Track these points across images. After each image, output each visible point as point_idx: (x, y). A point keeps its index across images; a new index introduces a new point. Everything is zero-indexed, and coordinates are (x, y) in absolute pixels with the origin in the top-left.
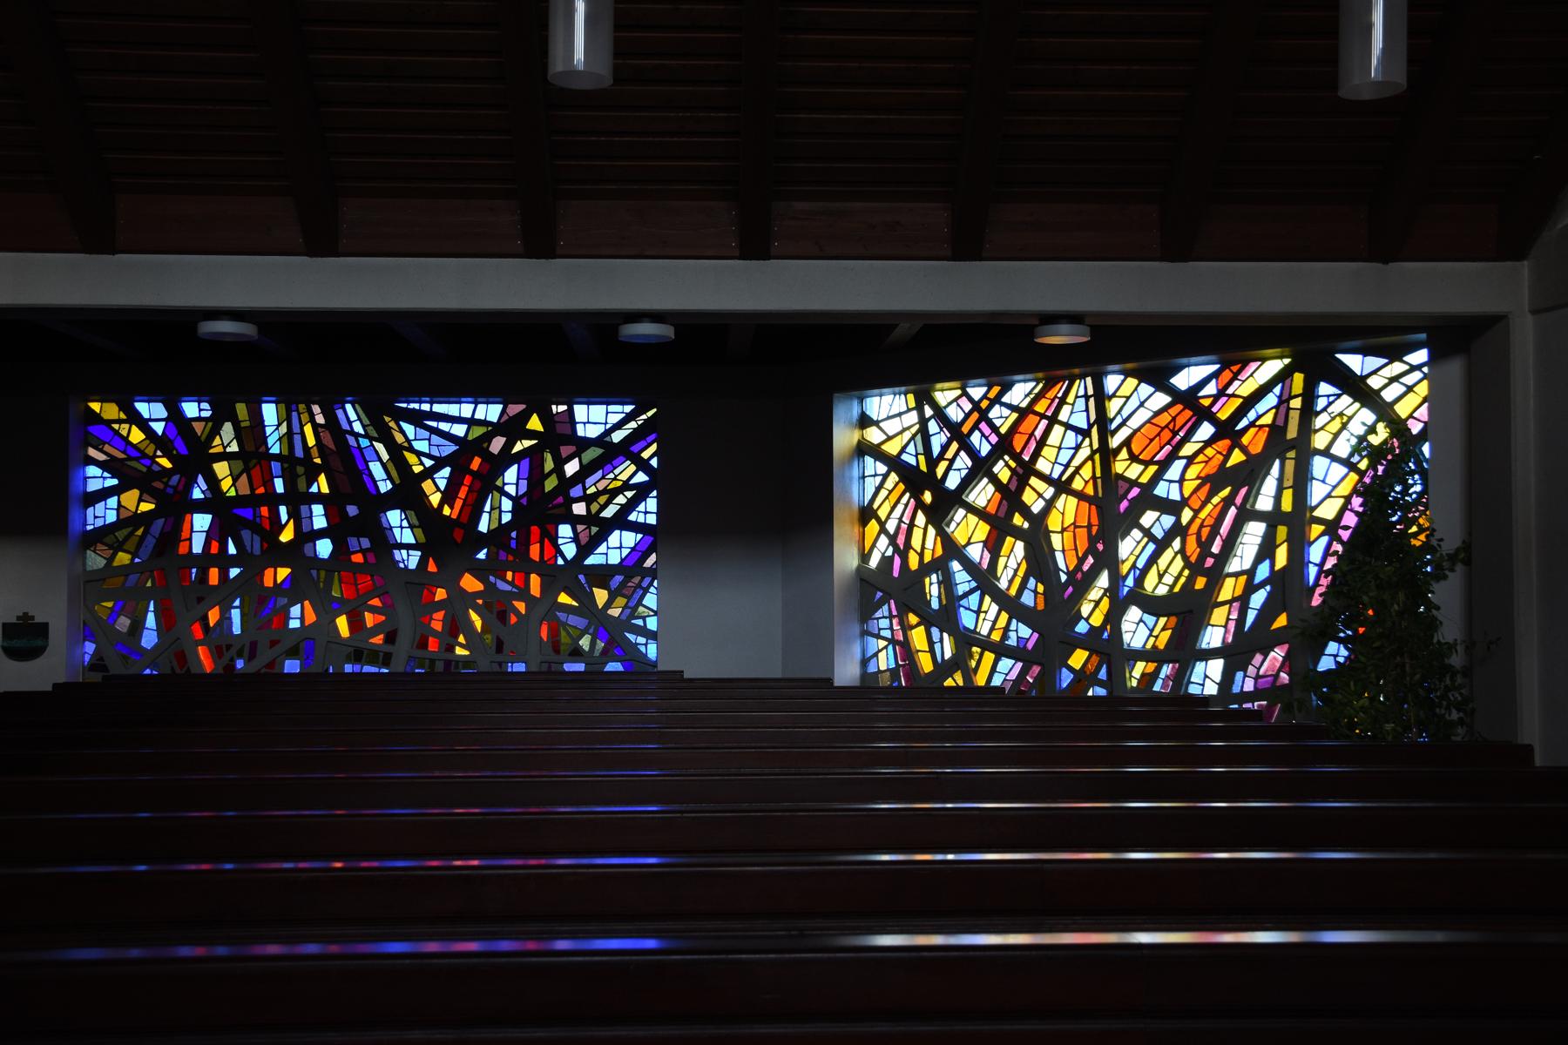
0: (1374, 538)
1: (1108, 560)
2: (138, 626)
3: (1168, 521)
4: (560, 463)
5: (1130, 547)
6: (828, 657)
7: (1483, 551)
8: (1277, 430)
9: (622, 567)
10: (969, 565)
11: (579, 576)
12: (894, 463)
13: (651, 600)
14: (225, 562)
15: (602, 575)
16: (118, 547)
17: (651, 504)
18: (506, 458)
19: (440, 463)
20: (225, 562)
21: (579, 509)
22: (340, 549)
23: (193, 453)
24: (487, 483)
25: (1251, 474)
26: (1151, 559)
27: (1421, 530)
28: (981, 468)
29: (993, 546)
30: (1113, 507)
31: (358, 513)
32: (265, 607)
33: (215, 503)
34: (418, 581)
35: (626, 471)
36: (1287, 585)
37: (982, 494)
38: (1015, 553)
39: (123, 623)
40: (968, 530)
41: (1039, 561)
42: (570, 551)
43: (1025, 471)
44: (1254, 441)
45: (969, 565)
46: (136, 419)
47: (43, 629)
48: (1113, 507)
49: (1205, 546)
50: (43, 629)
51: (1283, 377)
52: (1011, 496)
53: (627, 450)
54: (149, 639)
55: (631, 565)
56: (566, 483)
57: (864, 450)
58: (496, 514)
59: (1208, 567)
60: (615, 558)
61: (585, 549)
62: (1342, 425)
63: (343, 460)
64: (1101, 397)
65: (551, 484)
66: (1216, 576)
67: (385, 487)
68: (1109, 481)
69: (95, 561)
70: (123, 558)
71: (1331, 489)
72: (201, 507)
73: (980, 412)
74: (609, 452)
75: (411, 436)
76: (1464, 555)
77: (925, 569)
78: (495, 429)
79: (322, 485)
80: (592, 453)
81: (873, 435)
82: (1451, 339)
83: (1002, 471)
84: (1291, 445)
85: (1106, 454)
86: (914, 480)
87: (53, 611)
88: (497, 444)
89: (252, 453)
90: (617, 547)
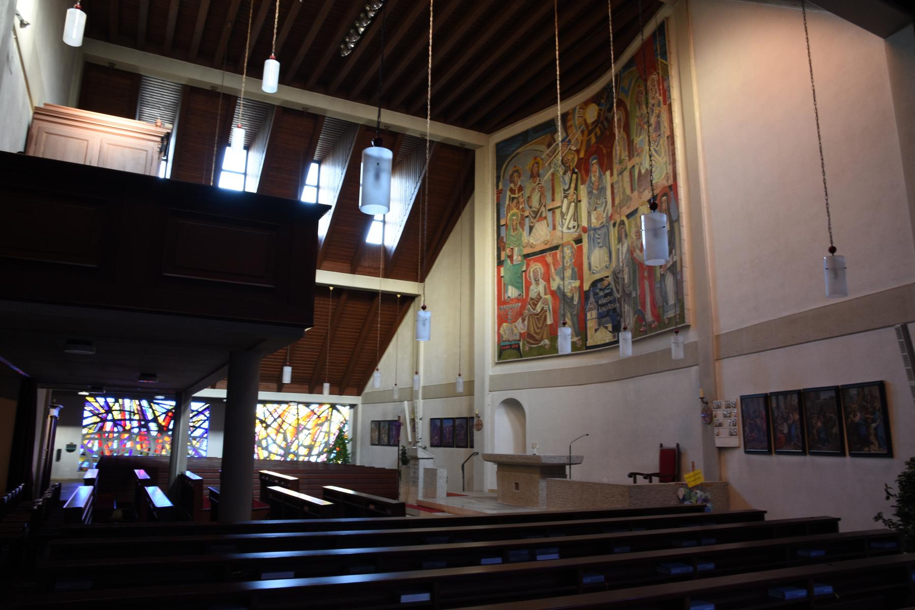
0: (340, 437)
1: (297, 438)
5: (301, 436)
7: (354, 440)
14: (113, 432)
15: (195, 438)
17: (207, 422)
20: (113, 432)
25: (321, 425)
26: (305, 439)
30: (298, 429)
31: (144, 423)
32: (122, 442)
33: (113, 420)
34: (156, 439)
35: (202, 417)
36: (327, 443)
37: (275, 425)
38: (281, 436)
41: (285, 439)
44: (323, 419)
46: (97, 401)
47: (75, 446)
48: (298, 429)
50: (75, 446)
52: (280, 426)
53: (202, 413)
55: (201, 437)
63: (142, 412)
68: (299, 424)
71: (335, 430)
72: (110, 421)
74: (199, 413)
76: (351, 440)
79: (137, 417)
80: (195, 413)
82: (352, 406)
87: (77, 442)
89: (122, 411)
90: (198, 432)
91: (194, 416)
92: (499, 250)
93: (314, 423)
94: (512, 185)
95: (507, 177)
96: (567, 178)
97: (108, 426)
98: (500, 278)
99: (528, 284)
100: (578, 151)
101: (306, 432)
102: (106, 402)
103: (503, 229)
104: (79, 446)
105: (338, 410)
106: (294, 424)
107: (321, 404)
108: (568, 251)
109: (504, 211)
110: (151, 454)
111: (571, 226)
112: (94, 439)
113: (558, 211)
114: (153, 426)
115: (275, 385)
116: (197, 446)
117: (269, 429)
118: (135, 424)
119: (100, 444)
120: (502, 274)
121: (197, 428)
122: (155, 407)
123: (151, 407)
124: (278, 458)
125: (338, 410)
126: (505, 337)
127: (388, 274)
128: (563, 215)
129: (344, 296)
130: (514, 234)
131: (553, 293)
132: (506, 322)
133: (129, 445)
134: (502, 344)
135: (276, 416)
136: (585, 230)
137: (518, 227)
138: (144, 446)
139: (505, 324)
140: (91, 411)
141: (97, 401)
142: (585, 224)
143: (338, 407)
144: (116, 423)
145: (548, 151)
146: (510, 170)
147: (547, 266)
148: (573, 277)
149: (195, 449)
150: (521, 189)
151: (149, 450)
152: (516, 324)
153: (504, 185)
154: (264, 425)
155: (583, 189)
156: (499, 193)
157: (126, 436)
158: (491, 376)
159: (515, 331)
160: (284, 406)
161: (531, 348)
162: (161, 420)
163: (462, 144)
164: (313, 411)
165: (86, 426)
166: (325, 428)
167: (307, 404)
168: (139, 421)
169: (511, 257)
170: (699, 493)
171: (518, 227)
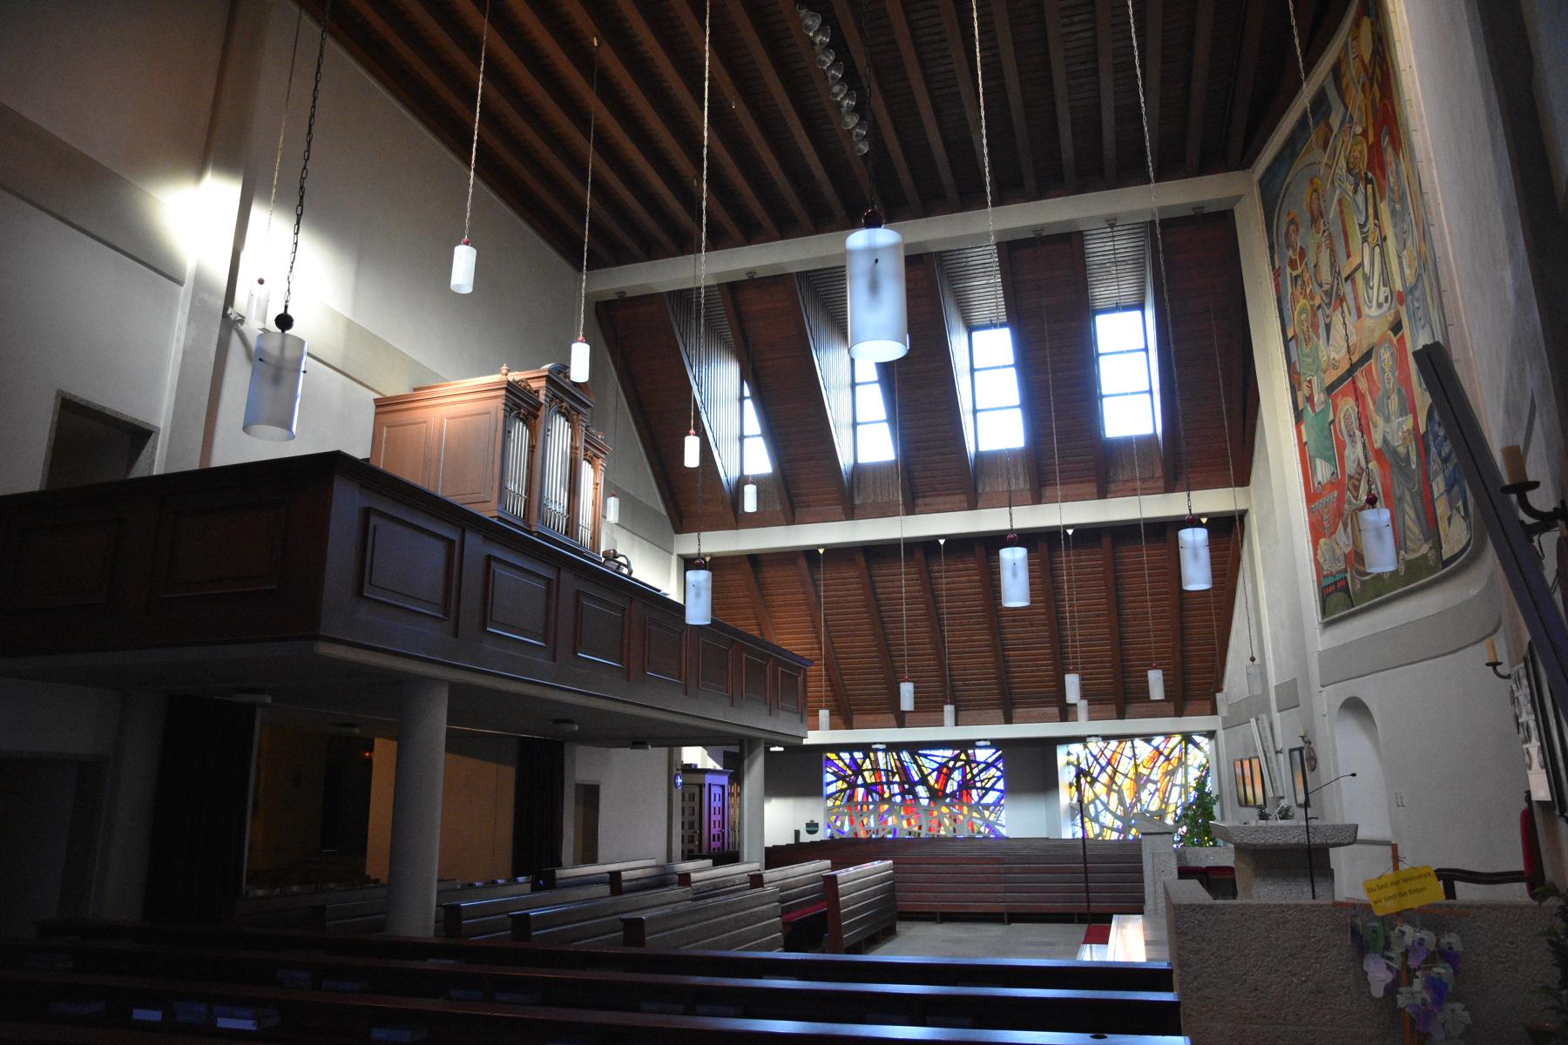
1: (1139, 800)
6: (1060, 832)
15: (987, 807)
18: (954, 768)
22: (903, 798)
23: (858, 770)
24: (948, 777)
25: (1172, 773)
28: (1103, 769)
29: (1108, 794)
30: (1140, 781)
32: (881, 818)
33: (865, 785)
34: (928, 811)
35: (993, 771)
37: (1104, 778)
38: (1114, 796)
40: (1100, 789)
41: (1121, 801)
43: (1115, 771)
44: (1174, 762)
52: (1112, 779)
55: (997, 803)
58: (952, 786)
61: (981, 798)
62: (1196, 758)
63: (903, 771)
66: (1167, 804)
67: (916, 779)
68: (1138, 774)
69: (830, 803)
74: (988, 766)
79: (897, 778)
82: (1211, 735)
83: (1109, 770)
84: (1182, 762)
85: (1136, 766)
87: (820, 819)
89: (875, 770)
90: (992, 797)
92: (1294, 389)
93: (1161, 771)
94: (1290, 253)
95: (1282, 240)
96: (1360, 198)
97: (860, 791)
98: (1302, 446)
99: (1341, 446)
100: (1364, 133)
101: (1151, 787)
102: (852, 758)
103: (1292, 345)
104: (821, 827)
105: (1196, 745)
106: (1131, 775)
107: (1168, 736)
108: (1385, 355)
109: (1287, 306)
111: (1382, 299)
112: (843, 814)
113: (1359, 276)
115: (1055, 710)
118: (896, 789)
119: (852, 822)
121: (987, 790)
122: (922, 761)
123: (916, 762)
124: (1115, 836)
125: (1196, 745)
126: (1326, 568)
127: (1171, 484)
128: (1367, 279)
129: (1106, 541)
130: (1307, 350)
131: (1379, 454)
132: (1324, 536)
133: (891, 821)
135: (1103, 762)
136: (1401, 299)
140: (834, 773)
142: (1398, 286)
143: (1197, 738)
145: (1325, 160)
146: (1284, 220)
147: (1359, 397)
148: (1403, 413)
150: (1302, 254)
153: (1281, 259)
155: (1384, 207)
156: (1277, 274)
157: (886, 807)
158: (1320, 653)
159: (1338, 553)
160: (1114, 744)
161: (1363, 583)
162: (932, 779)
163: (1198, 208)
164: (1157, 748)
165: (829, 797)
166: (1179, 779)
167: (1147, 738)
168: (901, 784)
169: (1310, 399)
170: (1411, 934)
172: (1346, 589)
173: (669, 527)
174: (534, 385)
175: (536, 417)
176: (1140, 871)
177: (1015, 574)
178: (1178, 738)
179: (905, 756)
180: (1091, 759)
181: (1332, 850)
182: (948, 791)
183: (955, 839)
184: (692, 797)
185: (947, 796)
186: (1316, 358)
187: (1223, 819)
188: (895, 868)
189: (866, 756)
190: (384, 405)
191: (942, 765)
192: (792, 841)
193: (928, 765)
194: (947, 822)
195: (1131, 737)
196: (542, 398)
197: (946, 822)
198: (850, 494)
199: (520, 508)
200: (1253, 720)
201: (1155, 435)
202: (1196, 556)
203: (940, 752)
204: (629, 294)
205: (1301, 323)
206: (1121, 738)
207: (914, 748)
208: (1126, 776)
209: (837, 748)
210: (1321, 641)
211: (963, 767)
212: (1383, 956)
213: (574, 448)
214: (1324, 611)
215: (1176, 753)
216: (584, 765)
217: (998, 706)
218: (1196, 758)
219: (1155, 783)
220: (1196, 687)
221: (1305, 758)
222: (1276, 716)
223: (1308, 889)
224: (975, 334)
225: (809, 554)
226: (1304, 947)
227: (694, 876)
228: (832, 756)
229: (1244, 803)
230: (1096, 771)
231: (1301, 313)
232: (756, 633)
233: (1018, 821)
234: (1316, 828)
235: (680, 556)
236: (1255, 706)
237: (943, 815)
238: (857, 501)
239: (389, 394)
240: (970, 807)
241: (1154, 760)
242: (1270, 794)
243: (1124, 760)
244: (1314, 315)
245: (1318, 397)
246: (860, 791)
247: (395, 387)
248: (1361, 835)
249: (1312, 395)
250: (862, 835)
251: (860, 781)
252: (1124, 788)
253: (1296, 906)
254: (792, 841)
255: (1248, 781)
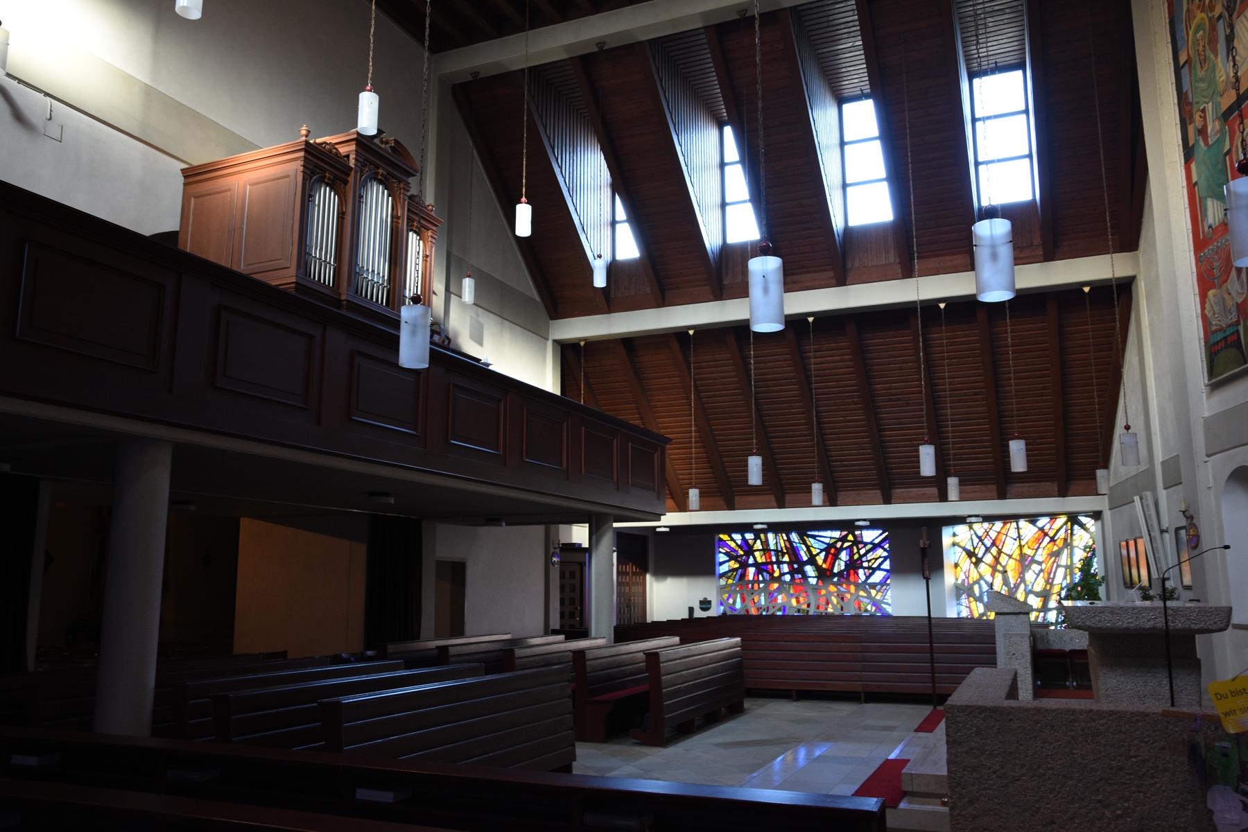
1: (1023, 580)
2: (735, 602)
3: (1039, 567)
4: (859, 550)
5: (1030, 576)
8: (1065, 540)
9: (879, 583)
10: (986, 582)
11: (951, 797)
12: (964, 549)
13: (889, 593)
14: (759, 582)
15: (873, 586)
16: (728, 578)
17: (888, 562)
18: (842, 549)
19: (822, 551)
21: (865, 564)
22: (793, 578)
23: (749, 550)
24: (836, 557)
25: (1057, 554)
27: (782, 574)
28: (987, 550)
29: (993, 575)
30: (1025, 562)
31: (797, 566)
32: (771, 596)
33: (756, 564)
34: (816, 589)
35: (880, 552)
37: (989, 559)
38: (999, 577)
39: (731, 601)
40: (985, 569)
41: (1006, 582)
42: (863, 578)
43: (1000, 552)
44: (1060, 543)
45: (986, 582)
46: (732, 539)
47: (710, 602)
48: (1025, 562)
49: (1049, 574)
50: (710, 602)
51: (1066, 523)
52: (997, 559)
53: (879, 545)
54: (738, 605)
55: (883, 583)
56: (861, 557)
57: (954, 544)
58: (839, 566)
59: (1050, 582)
60: (877, 581)
61: (868, 577)
62: (1082, 538)
63: (793, 551)
64: (1018, 528)
65: (856, 557)
66: (1052, 585)
67: (805, 558)
68: (1022, 555)
69: (722, 582)
70: (730, 581)
72: (752, 565)
73: (987, 533)
74: (875, 547)
75: (412, 285)
77: (975, 583)
78: (839, 540)
79: (786, 558)
80: (869, 547)
81: (957, 539)
82: (1097, 515)
83: (994, 550)
84: (1067, 543)
85: (1021, 547)
86: (970, 554)
87: (712, 597)
88: (839, 545)
89: (766, 550)
90: (878, 577)
91: (867, 552)
93: (1046, 551)
97: (752, 571)
98: (1191, 186)
101: (1035, 567)
103: (1185, 72)
104: (714, 604)
105: (1082, 526)
106: (1016, 555)
107: (1053, 516)
110: (811, 613)
114: (809, 570)
116: (878, 597)
117: (982, 565)
118: (785, 568)
119: (743, 600)
120: (1195, 179)
121: (874, 570)
122: (811, 541)
123: (805, 543)
125: (1082, 526)
130: (1201, 74)
132: (1213, 286)
134: (1212, 341)
137: (1208, 53)
138: (801, 599)
139: (1211, 293)
141: (732, 539)
143: (1083, 519)
144: (760, 568)
149: (875, 603)
151: (809, 605)
152: (1228, 285)
154: (974, 559)
157: (776, 586)
158: (1206, 419)
159: (1230, 303)
162: (820, 560)
164: (1042, 529)
165: (722, 575)
166: (1064, 560)
167: (1032, 518)
168: (790, 564)
169: (1202, 132)
171: (1208, 53)
172: (1237, 344)
173: (546, 316)
174: (343, 150)
175: (346, 182)
176: (994, 653)
177: (766, 290)
178: (1063, 519)
179: (794, 537)
180: (976, 540)
181: (1199, 638)
182: (836, 570)
183: (842, 617)
184: (573, 575)
185: (835, 575)
186: (1212, 81)
187: (1108, 598)
188: (743, 645)
189: (757, 537)
190: (193, 175)
191: (830, 546)
192: (686, 616)
193: (816, 546)
194: (834, 600)
195: (1015, 517)
196: (352, 163)
197: (833, 601)
198: (725, 276)
199: (328, 276)
200: (1137, 499)
201: (1034, 199)
202: (994, 256)
203: (828, 533)
204: (483, 75)
205: (1196, 42)
206: (1006, 518)
207: (804, 528)
208: (1010, 557)
209: (730, 529)
210: (1206, 405)
211: (850, 548)
212: (1237, 790)
213: (394, 217)
214: (1211, 372)
215: (1062, 534)
216: (445, 543)
217: (873, 487)
218: (1082, 538)
219: (1040, 563)
220: (1072, 457)
221: (1190, 535)
222: (1163, 494)
223: (1166, 681)
224: (846, 107)
225: (679, 335)
226: (1121, 769)
227: (452, 651)
228: (724, 537)
229: (1130, 584)
230: (980, 551)
231: (1196, 32)
232: (637, 422)
233: (902, 600)
234: (1176, 610)
235: (555, 341)
236: (1144, 482)
237: (831, 594)
238: (726, 282)
239: (196, 163)
240: (857, 586)
241: (1039, 541)
242: (1155, 575)
243: (1009, 541)
244: (1213, 29)
245: (1213, 127)
246: (752, 571)
247: (199, 158)
248: (1236, 619)
249: (1205, 126)
250: (753, 611)
251: (751, 561)
252: (1008, 569)
253: (1112, 713)
254: (686, 616)
255: (1133, 562)
